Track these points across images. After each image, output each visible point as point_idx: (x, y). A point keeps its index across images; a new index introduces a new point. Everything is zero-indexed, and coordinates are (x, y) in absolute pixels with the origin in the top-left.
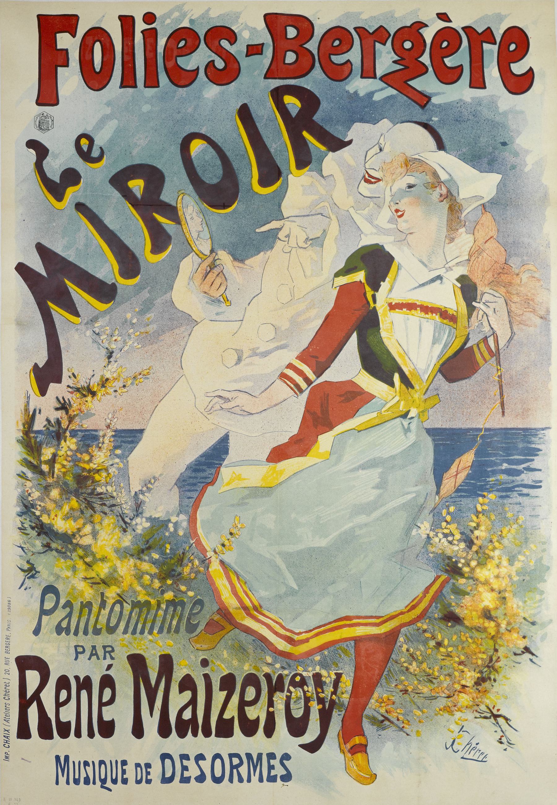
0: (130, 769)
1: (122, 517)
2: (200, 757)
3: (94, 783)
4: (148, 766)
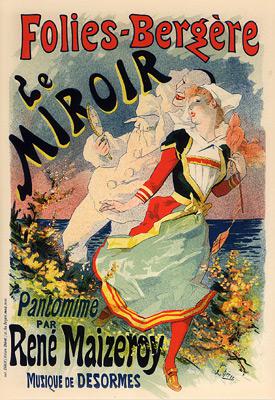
0: (63, 380)
1: (59, 261)
4: (72, 379)
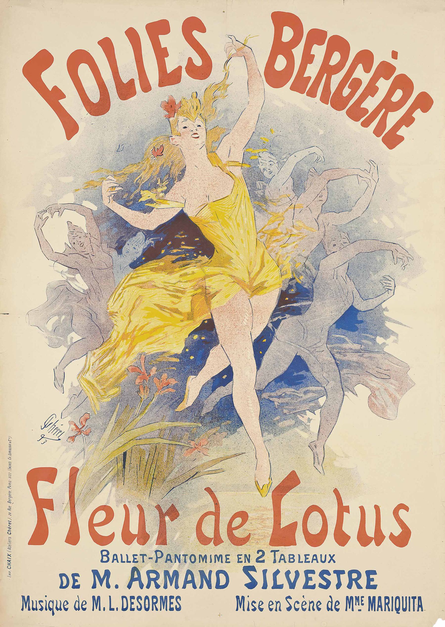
2: (139, 597)
3: (392, 610)
